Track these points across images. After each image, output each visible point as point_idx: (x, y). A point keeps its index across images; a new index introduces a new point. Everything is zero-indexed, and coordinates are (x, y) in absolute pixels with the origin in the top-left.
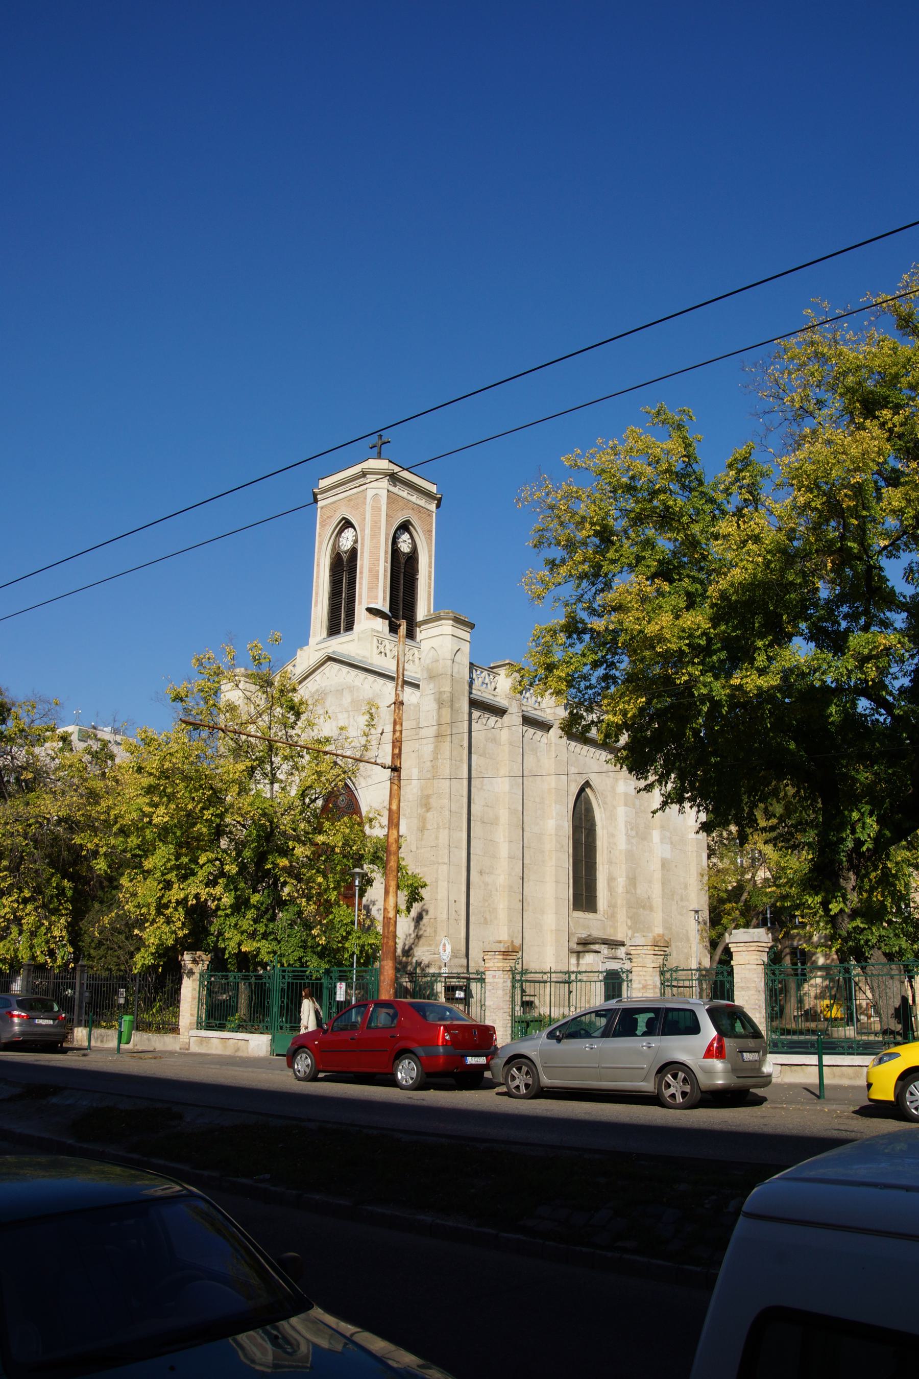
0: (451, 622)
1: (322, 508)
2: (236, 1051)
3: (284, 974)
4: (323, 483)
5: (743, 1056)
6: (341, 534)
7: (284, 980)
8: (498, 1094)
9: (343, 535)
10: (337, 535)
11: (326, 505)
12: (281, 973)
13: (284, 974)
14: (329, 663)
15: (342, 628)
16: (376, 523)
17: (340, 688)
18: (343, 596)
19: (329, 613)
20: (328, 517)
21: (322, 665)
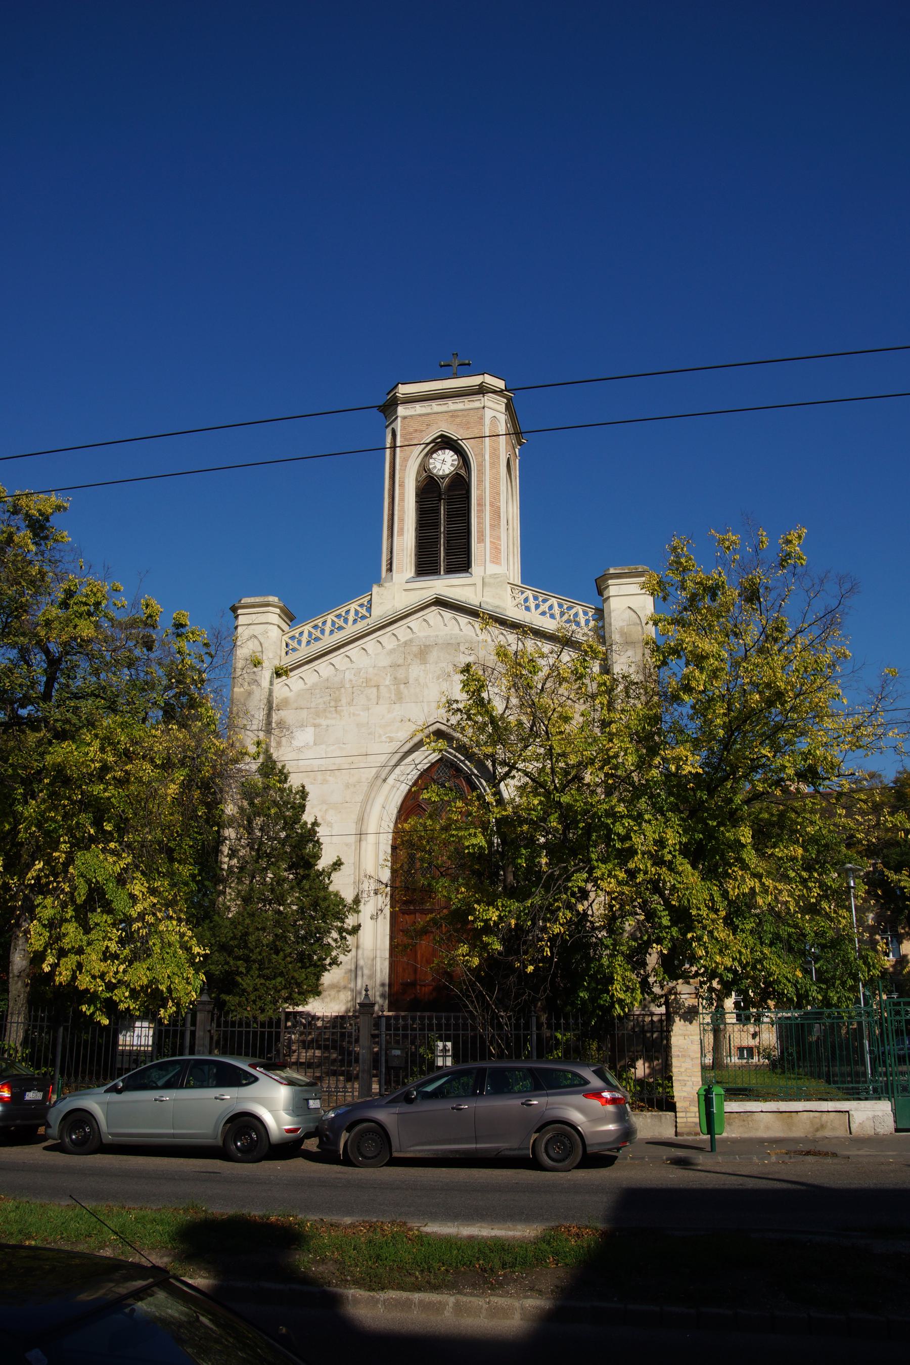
0: (278, 611)
1: (405, 418)
2: (817, 1130)
3: (897, 1008)
4: (404, 390)
5: (308, 1103)
6: (432, 454)
7: (898, 1018)
8: (46, 1148)
9: (434, 456)
10: (426, 455)
11: (411, 416)
12: (892, 1007)
13: (897, 1008)
14: (433, 608)
15: (442, 569)
16: (495, 450)
17: (453, 641)
18: (442, 530)
19: (416, 547)
20: (416, 431)
21: (422, 609)
